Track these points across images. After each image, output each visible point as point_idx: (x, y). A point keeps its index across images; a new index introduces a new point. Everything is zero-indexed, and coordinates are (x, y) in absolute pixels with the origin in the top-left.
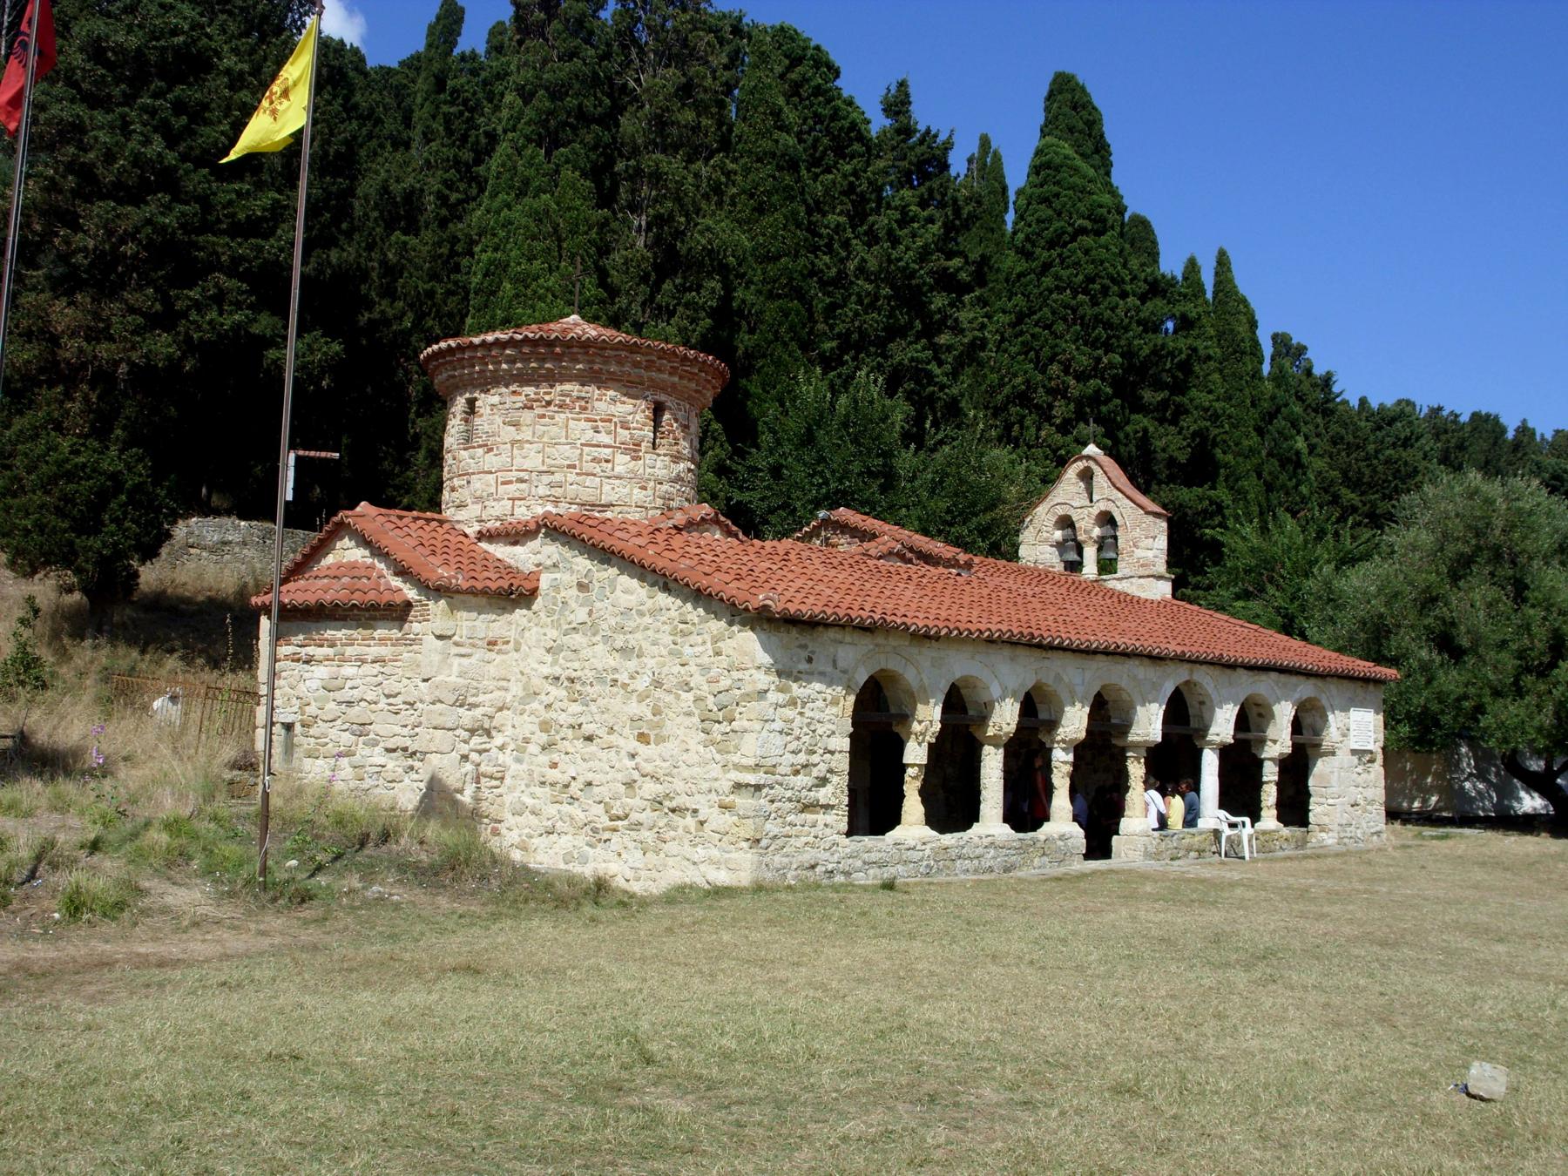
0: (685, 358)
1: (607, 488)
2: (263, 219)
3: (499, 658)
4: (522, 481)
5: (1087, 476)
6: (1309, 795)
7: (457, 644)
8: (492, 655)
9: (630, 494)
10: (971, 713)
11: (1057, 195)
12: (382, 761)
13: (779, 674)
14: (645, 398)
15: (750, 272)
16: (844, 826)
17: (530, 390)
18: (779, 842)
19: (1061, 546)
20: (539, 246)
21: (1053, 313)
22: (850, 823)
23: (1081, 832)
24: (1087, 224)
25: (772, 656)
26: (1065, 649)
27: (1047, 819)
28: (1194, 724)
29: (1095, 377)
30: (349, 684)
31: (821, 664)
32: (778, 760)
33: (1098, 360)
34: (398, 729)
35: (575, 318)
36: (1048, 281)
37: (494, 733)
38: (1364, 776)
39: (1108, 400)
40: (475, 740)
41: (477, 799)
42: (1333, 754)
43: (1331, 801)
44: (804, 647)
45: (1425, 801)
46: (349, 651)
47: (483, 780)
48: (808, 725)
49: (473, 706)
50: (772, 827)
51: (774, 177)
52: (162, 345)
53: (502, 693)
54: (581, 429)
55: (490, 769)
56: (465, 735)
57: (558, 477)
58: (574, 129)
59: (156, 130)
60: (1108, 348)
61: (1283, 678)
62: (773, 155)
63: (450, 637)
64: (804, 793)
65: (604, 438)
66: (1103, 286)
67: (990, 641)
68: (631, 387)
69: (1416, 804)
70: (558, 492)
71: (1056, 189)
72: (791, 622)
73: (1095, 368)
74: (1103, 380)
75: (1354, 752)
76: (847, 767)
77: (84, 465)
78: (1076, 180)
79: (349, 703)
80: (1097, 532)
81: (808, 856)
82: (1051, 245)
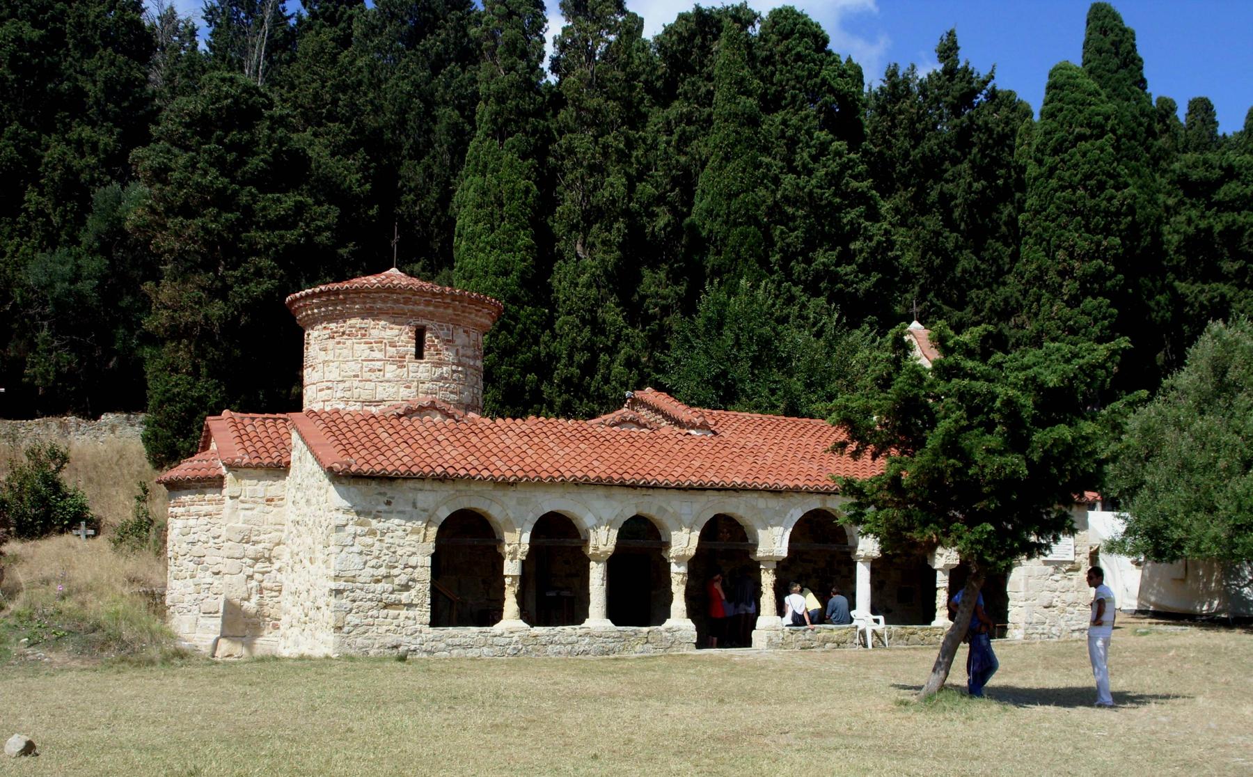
0: (434, 294)
1: (380, 389)
2: (288, 216)
3: (276, 510)
4: (329, 388)
6: (1007, 599)
7: (242, 502)
8: (271, 508)
9: (397, 392)
11: (1061, 110)
12: (209, 580)
13: (358, 513)
14: (409, 324)
15: (718, 208)
17: (333, 326)
18: (362, 629)
20: (482, 212)
21: (1058, 208)
24: (1088, 132)
25: (351, 502)
26: (667, 488)
28: (663, 539)
29: (1098, 257)
31: (398, 505)
32: (358, 572)
33: (1099, 244)
34: (219, 560)
35: (394, 271)
36: (1053, 182)
37: (274, 560)
38: (1065, 582)
39: (1113, 275)
40: (259, 566)
41: (261, 605)
44: (385, 494)
45: (1210, 605)
46: (193, 509)
47: (265, 592)
48: (388, 548)
49: (255, 543)
50: (352, 619)
51: (737, 133)
52: (217, 309)
53: (279, 534)
54: (362, 350)
56: (249, 562)
57: (347, 384)
58: (516, 122)
59: (212, 165)
60: (1107, 232)
62: (736, 115)
64: (385, 596)
66: (1099, 182)
67: (576, 483)
68: (396, 317)
69: (1205, 608)
70: (348, 394)
71: (1059, 105)
72: (358, 477)
73: (1097, 250)
74: (1105, 260)
77: (179, 393)
78: (1078, 95)
79: (193, 543)
81: (391, 639)
82: (1055, 152)
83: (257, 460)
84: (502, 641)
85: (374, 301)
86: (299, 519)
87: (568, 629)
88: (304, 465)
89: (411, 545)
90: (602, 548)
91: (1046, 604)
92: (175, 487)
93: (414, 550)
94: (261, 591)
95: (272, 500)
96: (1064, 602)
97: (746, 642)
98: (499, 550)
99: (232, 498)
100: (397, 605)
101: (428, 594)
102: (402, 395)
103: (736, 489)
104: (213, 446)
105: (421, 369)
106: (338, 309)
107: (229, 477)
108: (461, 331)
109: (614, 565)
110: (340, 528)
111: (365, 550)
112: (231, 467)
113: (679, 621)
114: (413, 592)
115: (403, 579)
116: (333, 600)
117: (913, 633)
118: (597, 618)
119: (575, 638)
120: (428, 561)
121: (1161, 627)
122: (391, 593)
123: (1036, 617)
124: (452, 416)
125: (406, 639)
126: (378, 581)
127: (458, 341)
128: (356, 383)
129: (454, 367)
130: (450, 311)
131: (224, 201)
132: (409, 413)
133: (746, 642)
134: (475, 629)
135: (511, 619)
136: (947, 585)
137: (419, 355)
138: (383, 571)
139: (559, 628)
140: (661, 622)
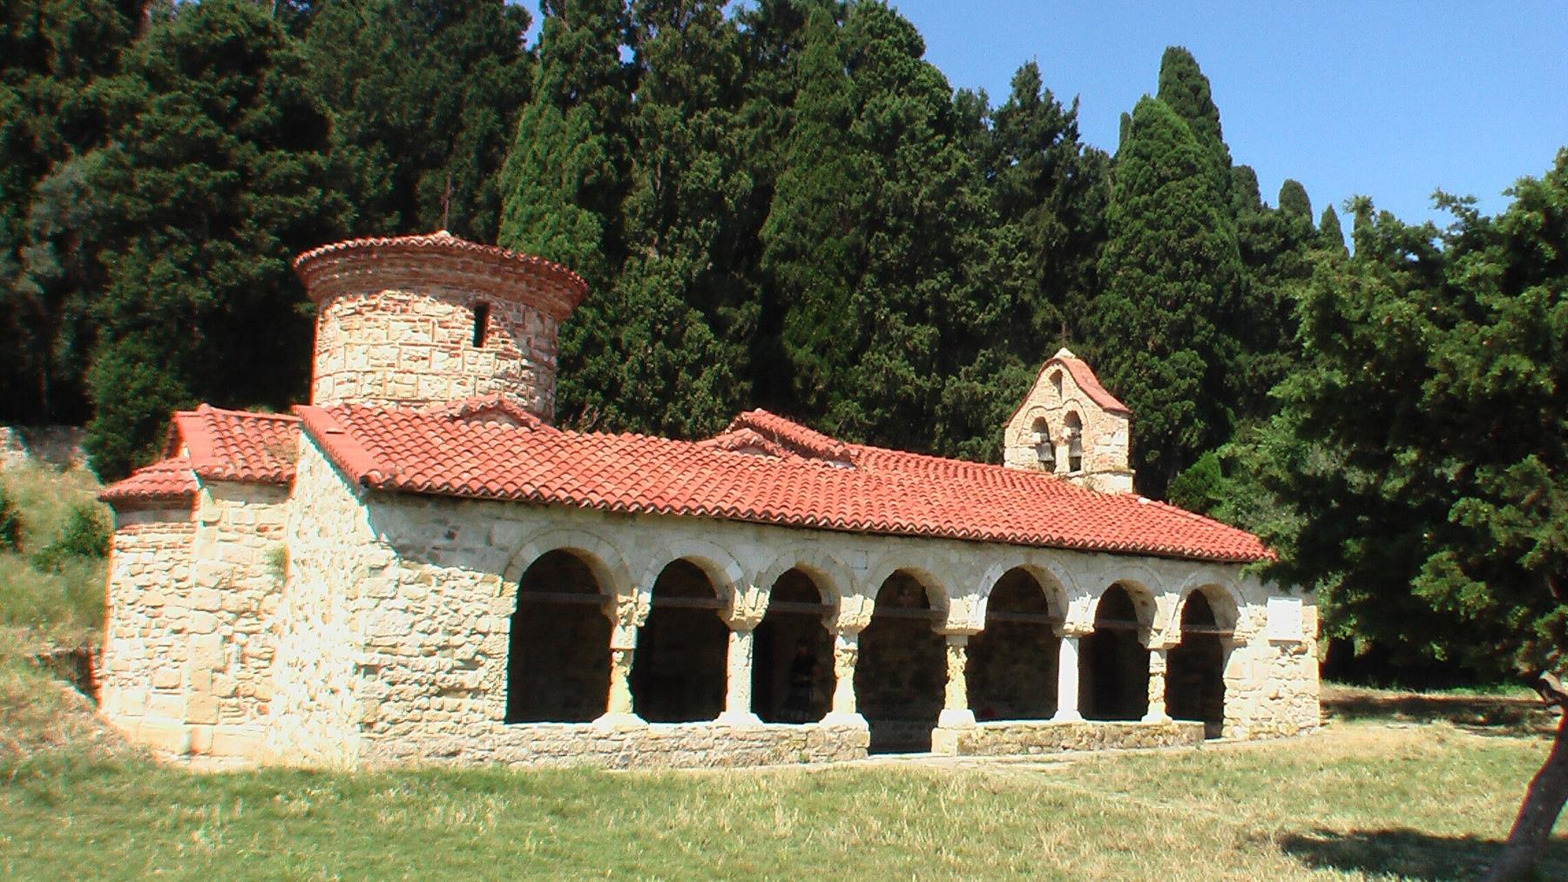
5: (1057, 378)
10: (933, 608)
16: (502, 712)
19: (1038, 447)
22: (510, 709)
23: (866, 724)
26: (840, 531)
27: (830, 710)
28: (1051, 612)
30: (147, 569)
32: (401, 640)
34: (184, 612)
35: (444, 233)
42: (1245, 645)
43: (1244, 694)
44: (443, 522)
49: (238, 590)
50: (391, 710)
54: (401, 328)
55: (256, 651)
56: (230, 617)
61: (1166, 564)
63: (214, 523)
64: (441, 675)
65: (424, 338)
68: (449, 292)
70: (378, 389)
75: (1274, 643)
76: (506, 650)
80: (1067, 432)
83: (247, 472)
84: (609, 745)
85: (422, 262)
86: (307, 556)
88: (315, 477)
89: (485, 605)
90: (749, 613)
92: (126, 506)
94: (242, 659)
95: (265, 529)
97: (924, 746)
98: (606, 612)
99: (206, 524)
101: (505, 674)
102: (459, 395)
103: (927, 537)
104: (184, 452)
106: (366, 281)
107: (204, 495)
108: (534, 315)
109: (764, 636)
110: (377, 569)
111: (413, 606)
112: (207, 479)
113: (845, 713)
114: (482, 671)
115: (468, 652)
116: (361, 681)
119: (710, 741)
120: (506, 625)
122: (449, 672)
124: (525, 423)
126: (430, 654)
127: (530, 327)
128: (389, 376)
129: (525, 362)
130: (523, 285)
131: (212, 155)
132: (468, 415)
133: (924, 746)
134: (570, 728)
136: (1164, 669)
137: (478, 342)
138: (439, 639)
139: (686, 726)
140: (817, 717)
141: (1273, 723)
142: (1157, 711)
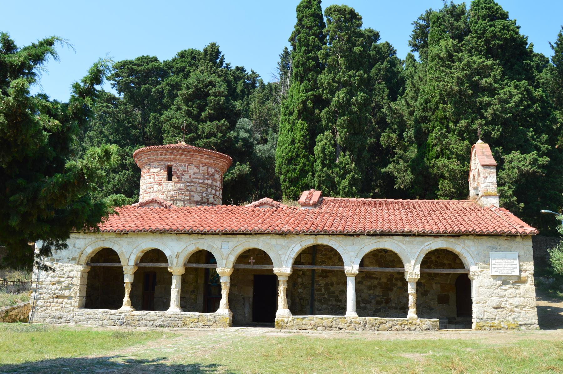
16: (77, 304)
18: (44, 308)
32: (43, 280)
48: (60, 267)
64: (56, 292)
75: (495, 277)
87: (152, 312)
91: (495, 306)
93: (72, 268)
96: (511, 304)
100: (63, 297)
105: (169, 185)
113: (223, 310)
115: (66, 283)
117: (383, 323)
118: (174, 308)
119: (156, 317)
120: (79, 274)
121: (460, 332)
123: (486, 315)
125: (66, 314)
126: (53, 284)
130: (183, 157)
135: (126, 307)
137: (169, 179)
138: (56, 279)
141: (496, 321)
142: (412, 313)
